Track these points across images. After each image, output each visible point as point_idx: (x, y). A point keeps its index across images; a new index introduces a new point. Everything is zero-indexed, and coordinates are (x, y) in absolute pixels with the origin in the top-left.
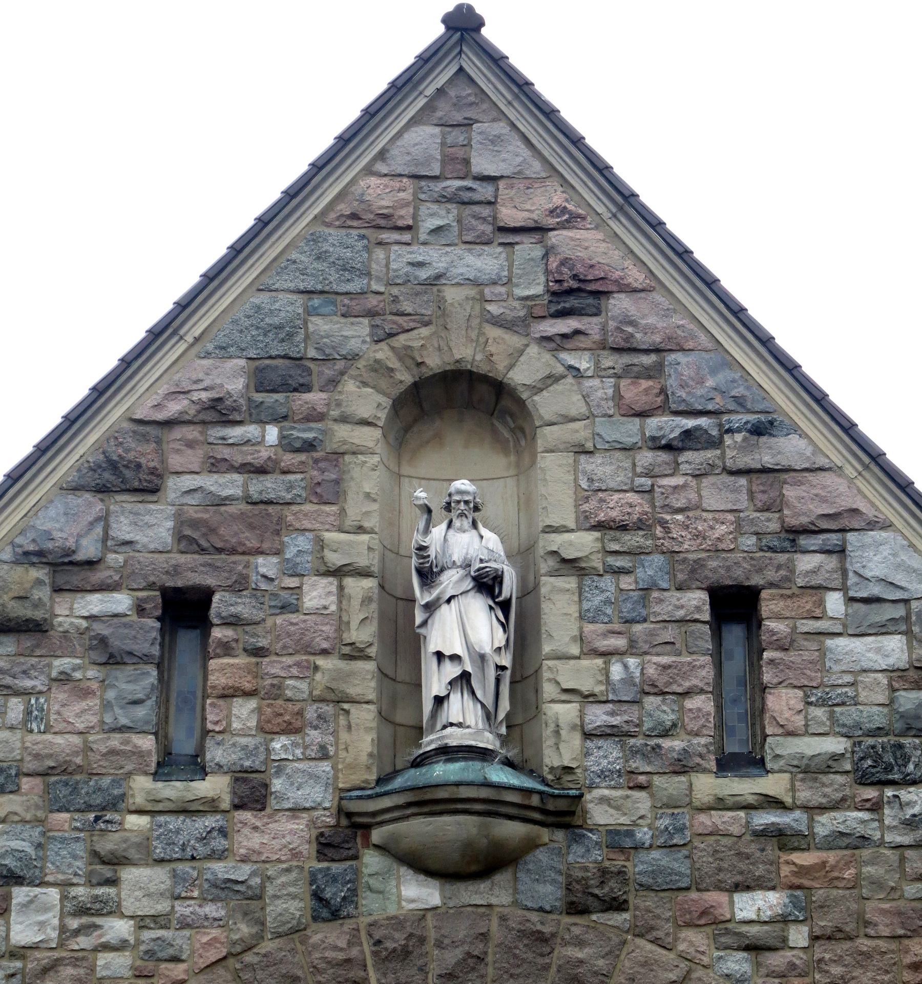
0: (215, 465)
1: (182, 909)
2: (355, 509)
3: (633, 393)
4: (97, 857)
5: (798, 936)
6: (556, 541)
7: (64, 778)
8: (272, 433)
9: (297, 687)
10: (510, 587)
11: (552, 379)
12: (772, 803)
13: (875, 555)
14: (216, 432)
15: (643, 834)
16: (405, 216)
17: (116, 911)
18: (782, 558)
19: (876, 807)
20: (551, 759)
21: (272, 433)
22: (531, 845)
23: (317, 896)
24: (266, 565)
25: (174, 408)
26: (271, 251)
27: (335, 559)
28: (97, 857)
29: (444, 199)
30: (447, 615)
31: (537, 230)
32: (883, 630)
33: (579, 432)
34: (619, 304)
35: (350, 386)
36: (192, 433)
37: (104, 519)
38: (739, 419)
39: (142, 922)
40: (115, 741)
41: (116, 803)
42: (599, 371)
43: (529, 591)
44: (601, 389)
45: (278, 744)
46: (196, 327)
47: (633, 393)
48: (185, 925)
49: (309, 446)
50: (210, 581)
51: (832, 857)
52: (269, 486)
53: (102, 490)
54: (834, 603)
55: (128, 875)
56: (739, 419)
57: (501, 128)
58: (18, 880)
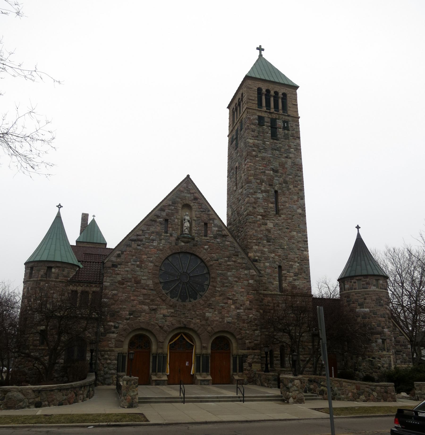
0: (169, 210)
1: (166, 244)
2: (179, 214)
3: (200, 207)
4: (160, 239)
5: (209, 249)
6: (194, 218)
7: (240, 250)
8: (173, 207)
9: (175, 227)
11: (194, 205)
12: (208, 239)
13: (259, 198)
15: (199, 241)
16: (183, 191)
17: (161, 243)
18: (260, 185)
19: (215, 240)
20: (193, 235)
21: (173, 207)
22: (191, 241)
23: (176, 244)
24: (173, 218)
25: (166, 205)
26: (173, 193)
27: (178, 218)
28: (160, 239)
30: (186, 223)
31: (193, 193)
32: (216, 227)
33: (195, 210)
34: (199, 200)
35: (179, 204)
36: (167, 207)
37: (161, 213)
38: (207, 210)
39: (163, 244)
40: (161, 230)
41: (161, 235)
43: (191, 221)
44: (197, 207)
45: (173, 232)
46: (168, 198)
47: (200, 207)
48: (166, 245)
49: (176, 209)
51: (212, 244)
52: (173, 212)
53: (160, 211)
54: (213, 225)
55: (162, 241)
56: (207, 210)
57: (191, 185)
58: (154, 240)
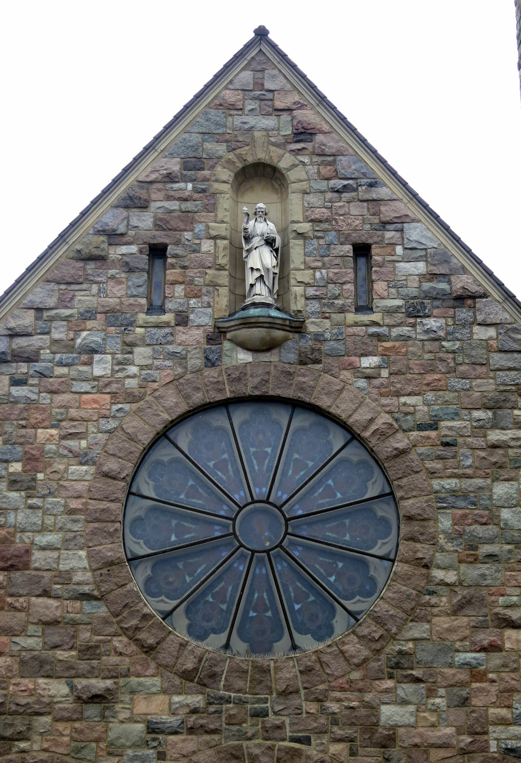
0: (169, 198)
8: (190, 186)
21: (190, 186)
42: (312, 163)
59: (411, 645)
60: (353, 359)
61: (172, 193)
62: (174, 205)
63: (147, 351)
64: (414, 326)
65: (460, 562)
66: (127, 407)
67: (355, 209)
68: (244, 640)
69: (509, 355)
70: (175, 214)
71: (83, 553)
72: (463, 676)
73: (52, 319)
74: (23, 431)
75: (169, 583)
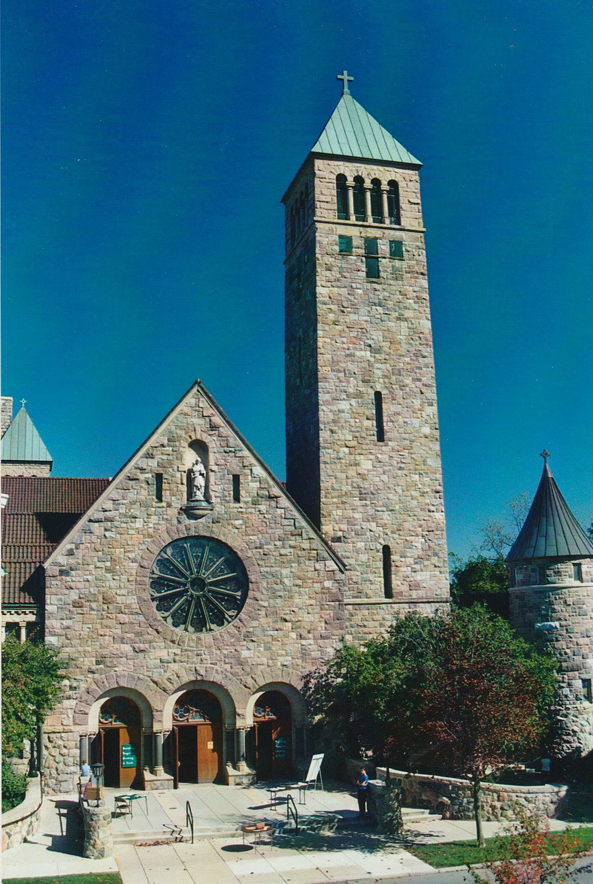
0: (162, 454)
8: (171, 449)
10: (205, 475)
14: (163, 448)
21: (171, 449)
29: (196, 410)
32: (256, 481)
42: (218, 440)
50: (162, 472)
59: (252, 629)
60: (232, 521)
61: (165, 452)
62: (165, 457)
63: (156, 517)
64: (255, 508)
65: (269, 598)
66: (149, 540)
67: (235, 461)
68: (193, 627)
69: (288, 520)
70: (165, 461)
71: (135, 597)
72: (270, 639)
73: (119, 504)
74: (110, 550)
75: (164, 606)
